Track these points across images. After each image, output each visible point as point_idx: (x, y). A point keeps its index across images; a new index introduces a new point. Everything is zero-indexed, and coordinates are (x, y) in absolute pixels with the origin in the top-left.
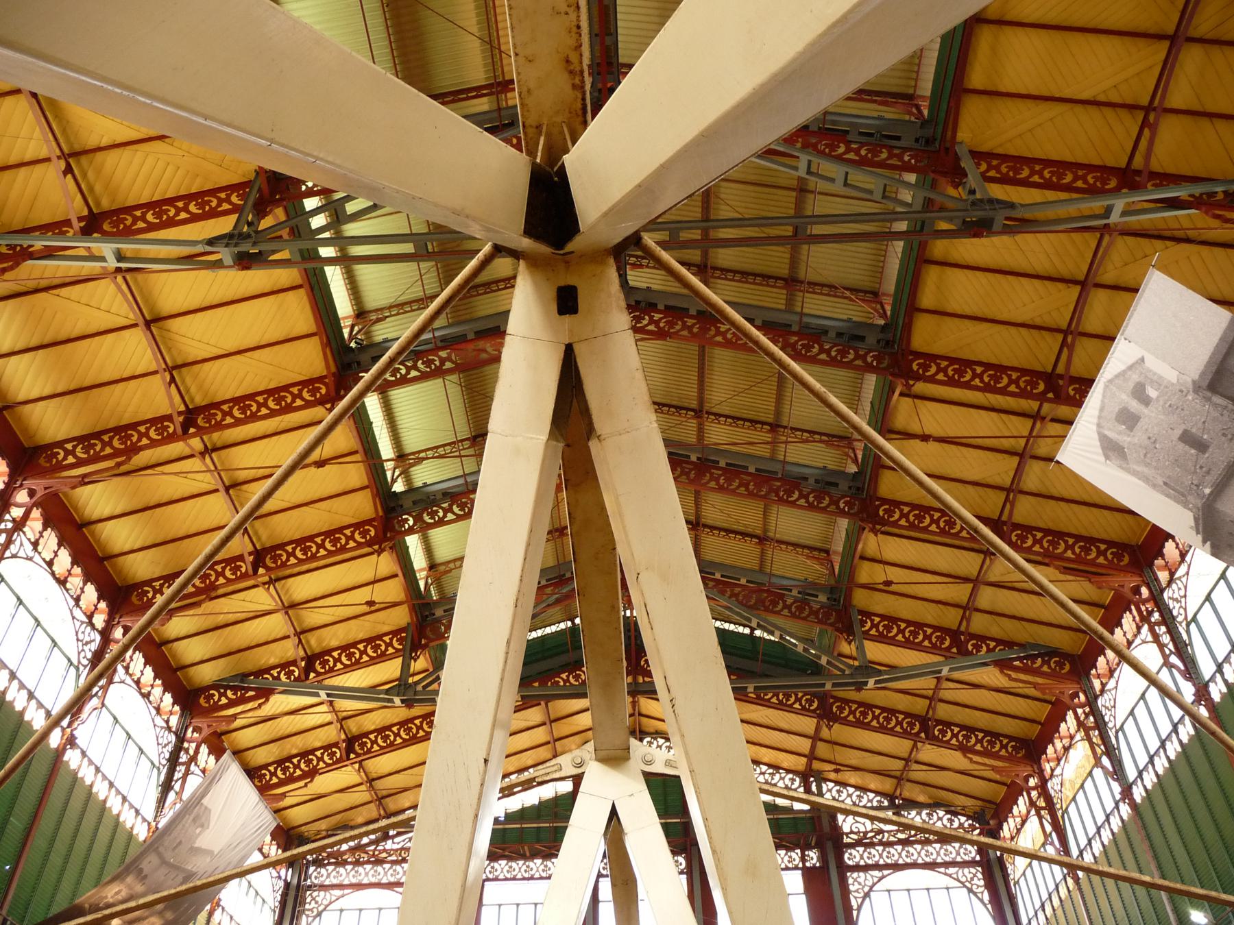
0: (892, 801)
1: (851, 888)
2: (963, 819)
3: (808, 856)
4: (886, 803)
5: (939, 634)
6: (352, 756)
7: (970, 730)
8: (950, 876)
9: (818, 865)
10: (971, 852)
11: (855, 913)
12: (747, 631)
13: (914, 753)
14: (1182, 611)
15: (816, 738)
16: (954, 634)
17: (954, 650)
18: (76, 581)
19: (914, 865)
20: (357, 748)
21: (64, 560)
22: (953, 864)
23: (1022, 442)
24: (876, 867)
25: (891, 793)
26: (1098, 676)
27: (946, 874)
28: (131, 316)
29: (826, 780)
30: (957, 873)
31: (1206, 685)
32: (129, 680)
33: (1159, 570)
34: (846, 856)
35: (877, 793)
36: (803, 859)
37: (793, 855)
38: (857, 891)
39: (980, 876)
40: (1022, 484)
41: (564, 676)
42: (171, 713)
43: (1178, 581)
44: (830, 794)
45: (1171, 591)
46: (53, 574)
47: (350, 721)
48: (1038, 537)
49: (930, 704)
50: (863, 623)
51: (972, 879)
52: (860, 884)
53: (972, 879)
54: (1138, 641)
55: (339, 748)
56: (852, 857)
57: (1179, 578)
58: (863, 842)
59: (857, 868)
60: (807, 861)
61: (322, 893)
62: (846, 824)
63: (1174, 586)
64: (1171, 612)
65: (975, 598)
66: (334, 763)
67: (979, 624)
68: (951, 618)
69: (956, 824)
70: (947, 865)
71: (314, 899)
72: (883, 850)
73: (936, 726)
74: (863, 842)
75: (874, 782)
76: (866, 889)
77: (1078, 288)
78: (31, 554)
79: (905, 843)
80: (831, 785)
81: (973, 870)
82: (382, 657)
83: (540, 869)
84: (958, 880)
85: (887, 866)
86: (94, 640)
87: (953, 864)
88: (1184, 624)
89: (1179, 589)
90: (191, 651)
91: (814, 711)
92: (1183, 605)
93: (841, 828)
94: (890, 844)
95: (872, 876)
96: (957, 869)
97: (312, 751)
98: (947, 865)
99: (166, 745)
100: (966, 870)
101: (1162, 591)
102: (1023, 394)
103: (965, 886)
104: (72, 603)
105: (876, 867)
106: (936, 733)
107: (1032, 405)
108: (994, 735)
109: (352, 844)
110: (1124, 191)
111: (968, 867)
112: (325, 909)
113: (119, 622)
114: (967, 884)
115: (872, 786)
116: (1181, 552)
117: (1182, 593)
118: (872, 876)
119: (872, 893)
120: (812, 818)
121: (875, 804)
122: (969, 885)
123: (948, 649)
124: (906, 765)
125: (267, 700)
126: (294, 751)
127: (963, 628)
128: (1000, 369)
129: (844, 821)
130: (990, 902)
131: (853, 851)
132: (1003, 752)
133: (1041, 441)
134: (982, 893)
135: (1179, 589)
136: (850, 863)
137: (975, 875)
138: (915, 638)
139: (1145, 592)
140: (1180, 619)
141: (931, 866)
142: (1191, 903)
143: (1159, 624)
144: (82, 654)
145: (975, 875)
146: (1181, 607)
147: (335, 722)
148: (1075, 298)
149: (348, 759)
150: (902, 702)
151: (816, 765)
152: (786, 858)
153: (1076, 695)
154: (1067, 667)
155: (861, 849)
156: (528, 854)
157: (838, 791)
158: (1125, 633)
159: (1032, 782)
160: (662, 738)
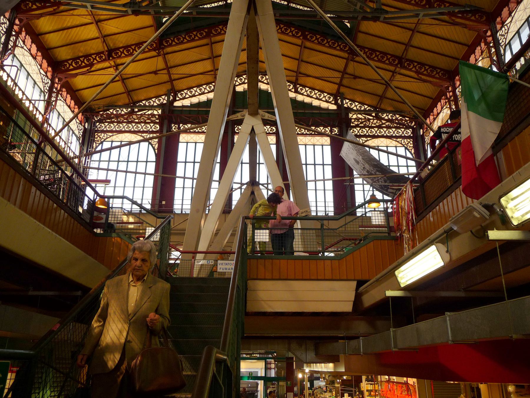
3: (334, 130)
6: (111, 58)
7: (422, 64)
8: (398, 142)
10: (409, 132)
14: (504, 40)
15: (344, 72)
17: (427, 6)
18: (39, 58)
19: (383, 136)
20: (113, 55)
21: (34, 49)
22: (400, 137)
23: (414, 25)
24: (112, 131)
25: (375, 106)
26: (433, 115)
27: (396, 141)
28: (104, 25)
30: (401, 141)
32: (62, 99)
33: (498, 24)
34: (236, 128)
36: (331, 131)
37: (327, 129)
39: (411, 142)
40: (412, 42)
42: (74, 108)
44: (347, 103)
45: (501, 31)
46: (31, 54)
47: (108, 38)
49: (406, 48)
51: (408, 144)
53: (408, 144)
54: (445, 107)
55: (104, 55)
56: (156, 127)
57: (506, 25)
60: (333, 132)
61: (103, 134)
62: (353, 116)
63: (503, 29)
64: (499, 41)
65: (386, 93)
66: (102, 61)
67: (412, 54)
68: (399, 50)
70: (396, 137)
71: (409, 142)
72: (369, 130)
73: (406, 62)
75: (368, 99)
76: (102, 140)
77: (411, 32)
78: (23, 45)
80: (347, 101)
81: (409, 140)
83: (269, 130)
84: (401, 144)
86: (48, 83)
87: (400, 137)
90: (53, 40)
91: (347, 51)
92: (506, 37)
94: (373, 127)
95: (362, 140)
96: (401, 139)
97: (91, 55)
98: (396, 137)
99: (81, 130)
100: (405, 140)
101: (497, 32)
102: (390, 64)
104: (39, 67)
105: (112, 131)
106: (406, 65)
107: (392, 68)
108: (433, 68)
111: (407, 139)
112: (104, 141)
113: (57, 76)
114: (405, 146)
115: (367, 103)
116: (476, 59)
118: (362, 140)
120: (338, 113)
122: (406, 146)
123: (425, 5)
124: (393, 75)
126: (81, 54)
127: (378, 106)
128: (385, 54)
130: (414, 153)
131: (139, 125)
132: (437, 76)
133: (422, 26)
134: (411, 149)
135: (505, 30)
138: (383, 59)
139: (450, 89)
140: (427, 142)
141: (390, 137)
143: (452, 101)
144: (45, 88)
146: (504, 38)
147: (101, 37)
148: (410, 35)
149: (109, 59)
151: (342, 90)
153: (486, 32)
154: (484, 18)
155: (358, 129)
156: (201, 122)
158: (475, 56)
159: (489, 33)
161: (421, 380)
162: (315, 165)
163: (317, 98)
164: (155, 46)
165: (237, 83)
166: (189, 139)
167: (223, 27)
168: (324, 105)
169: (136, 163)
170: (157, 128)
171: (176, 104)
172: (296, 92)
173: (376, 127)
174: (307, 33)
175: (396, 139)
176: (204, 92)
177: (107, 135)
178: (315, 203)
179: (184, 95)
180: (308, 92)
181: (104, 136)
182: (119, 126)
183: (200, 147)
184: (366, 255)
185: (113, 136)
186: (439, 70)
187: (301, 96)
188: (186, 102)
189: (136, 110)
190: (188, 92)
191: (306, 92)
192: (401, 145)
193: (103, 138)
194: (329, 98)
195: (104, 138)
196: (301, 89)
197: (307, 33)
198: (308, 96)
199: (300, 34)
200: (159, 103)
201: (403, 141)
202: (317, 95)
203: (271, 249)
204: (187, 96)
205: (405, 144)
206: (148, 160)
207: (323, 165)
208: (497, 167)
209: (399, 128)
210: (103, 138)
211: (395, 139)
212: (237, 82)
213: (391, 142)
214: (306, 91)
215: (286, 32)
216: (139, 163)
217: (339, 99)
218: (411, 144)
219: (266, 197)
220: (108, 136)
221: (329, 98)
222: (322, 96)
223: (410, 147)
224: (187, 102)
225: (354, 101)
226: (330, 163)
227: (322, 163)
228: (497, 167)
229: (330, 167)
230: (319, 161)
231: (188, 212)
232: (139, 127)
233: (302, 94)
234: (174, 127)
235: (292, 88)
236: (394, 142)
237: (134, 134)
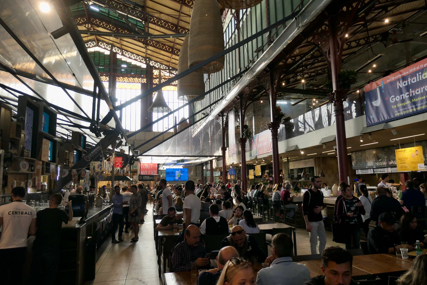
0: (169, 68)
4: (167, 68)
5: (172, 26)
9: (146, 83)
12: (126, 15)
16: (176, 26)
29: (152, 60)
34: (154, 81)
35: (165, 65)
41: (79, 19)
50: (151, 19)
73: (176, 50)
83: (105, 79)
93: (154, 74)
109: (313, 66)
110: (349, 28)
121: (164, 68)
131: (156, 80)
136: (155, 83)
142: (300, 81)
150: (168, 44)
152: (137, 80)
160: (105, 43)
161: (345, 119)
163: (135, 60)
164: (85, 20)
167: (80, 19)
168: (138, 64)
172: (122, 54)
174: (119, 29)
179: (89, 45)
180: (130, 55)
184: (396, 68)
187: (125, 57)
190: (92, 43)
191: (128, 55)
196: (125, 53)
197: (119, 29)
198: (130, 58)
199: (115, 29)
202: (135, 57)
203: (44, 140)
204: (91, 46)
208: (296, 83)
212: (91, 45)
215: (107, 28)
219: (157, 92)
222: (138, 58)
228: (296, 83)
232: (156, 81)
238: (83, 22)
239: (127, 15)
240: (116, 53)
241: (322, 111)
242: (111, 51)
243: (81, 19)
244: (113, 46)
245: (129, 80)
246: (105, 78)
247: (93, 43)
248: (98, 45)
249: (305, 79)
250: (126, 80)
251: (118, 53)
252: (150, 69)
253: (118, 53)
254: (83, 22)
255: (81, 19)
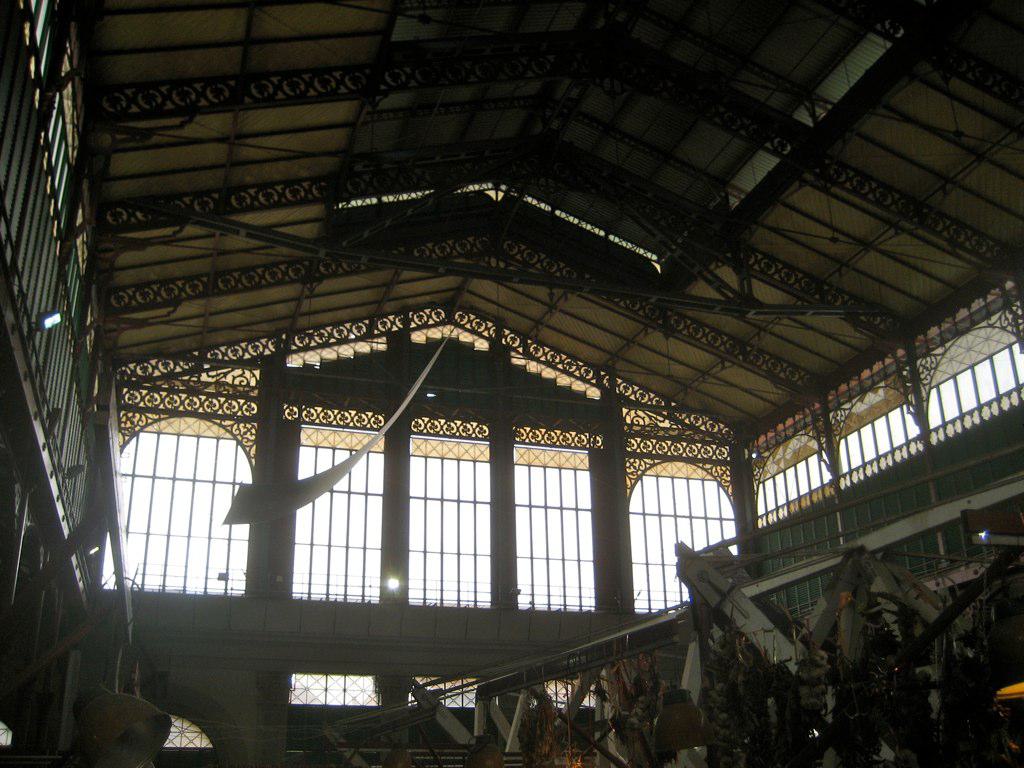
0: (668, 404)
1: (242, 425)
2: (722, 426)
11: (628, 491)
13: (642, 335)
19: (194, 414)
22: (709, 461)
24: (649, 455)
27: (220, 425)
30: (232, 426)
31: (930, 431)
38: (632, 473)
43: (933, 358)
48: (850, 175)
51: (245, 433)
52: (635, 468)
53: (245, 433)
57: (935, 355)
58: (645, 433)
59: (634, 454)
62: (629, 416)
69: (716, 430)
70: (704, 461)
74: (645, 433)
79: (676, 439)
82: (332, 96)
84: (231, 432)
85: (658, 456)
87: (709, 461)
88: (927, 387)
89: (932, 362)
95: (645, 463)
96: (231, 423)
98: (704, 461)
103: (716, 480)
105: (649, 455)
114: (239, 438)
115: (654, 387)
117: (933, 366)
118: (645, 463)
119: (141, 434)
125: (190, 121)
129: (627, 414)
130: (256, 456)
137: (725, 472)
145: (725, 472)
146: (929, 374)
157: (478, 324)
162: (442, 500)
165: (413, 325)
166: (332, 436)
169: (657, 513)
170: (253, 409)
171: (295, 362)
172: (527, 355)
173: (671, 438)
175: (222, 420)
176: (347, 337)
177: (147, 418)
178: (473, 594)
181: (140, 420)
182: (173, 399)
183: (585, 478)
185: (160, 420)
186: (689, 322)
188: (311, 357)
189: (206, 366)
192: (230, 436)
193: (138, 425)
194: (587, 372)
195: (140, 423)
200: (255, 354)
201: (236, 426)
205: (240, 434)
206: (543, 504)
207: (366, 494)
209: (709, 444)
210: (138, 425)
211: (219, 421)
213: (209, 428)
214: (545, 354)
216: (574, 512)
217: (604, 376)
218: (252, 434)
220: (150, 421)
221: (587, 372)
223: (248, 440)
224: (313, 358)
225: (631, 383)
226: (381, 492)
227: (364, 491)
229: (589, 515)
230: (466, 494)
231: (488, 605)
233: (538, 360)
234: (287, 411)
235: (519, 346)
236: (699, 471)
237: (206, 419)
238: (183, 104)
239: (553, 210)
240: (509, 348)
241: (588, 552)
242: (494, 342)
243: (174, 92)
244: (500, 325)
245: (535, 436)
246: (576, 439)
247: (438, 314)
248: (449, 320)
249: (976, 658)
250: (528, 434)
251: (515, 350)
252: (613, 402)
253: (515, 350)
254: (183, 104)
255: (174, 92)
